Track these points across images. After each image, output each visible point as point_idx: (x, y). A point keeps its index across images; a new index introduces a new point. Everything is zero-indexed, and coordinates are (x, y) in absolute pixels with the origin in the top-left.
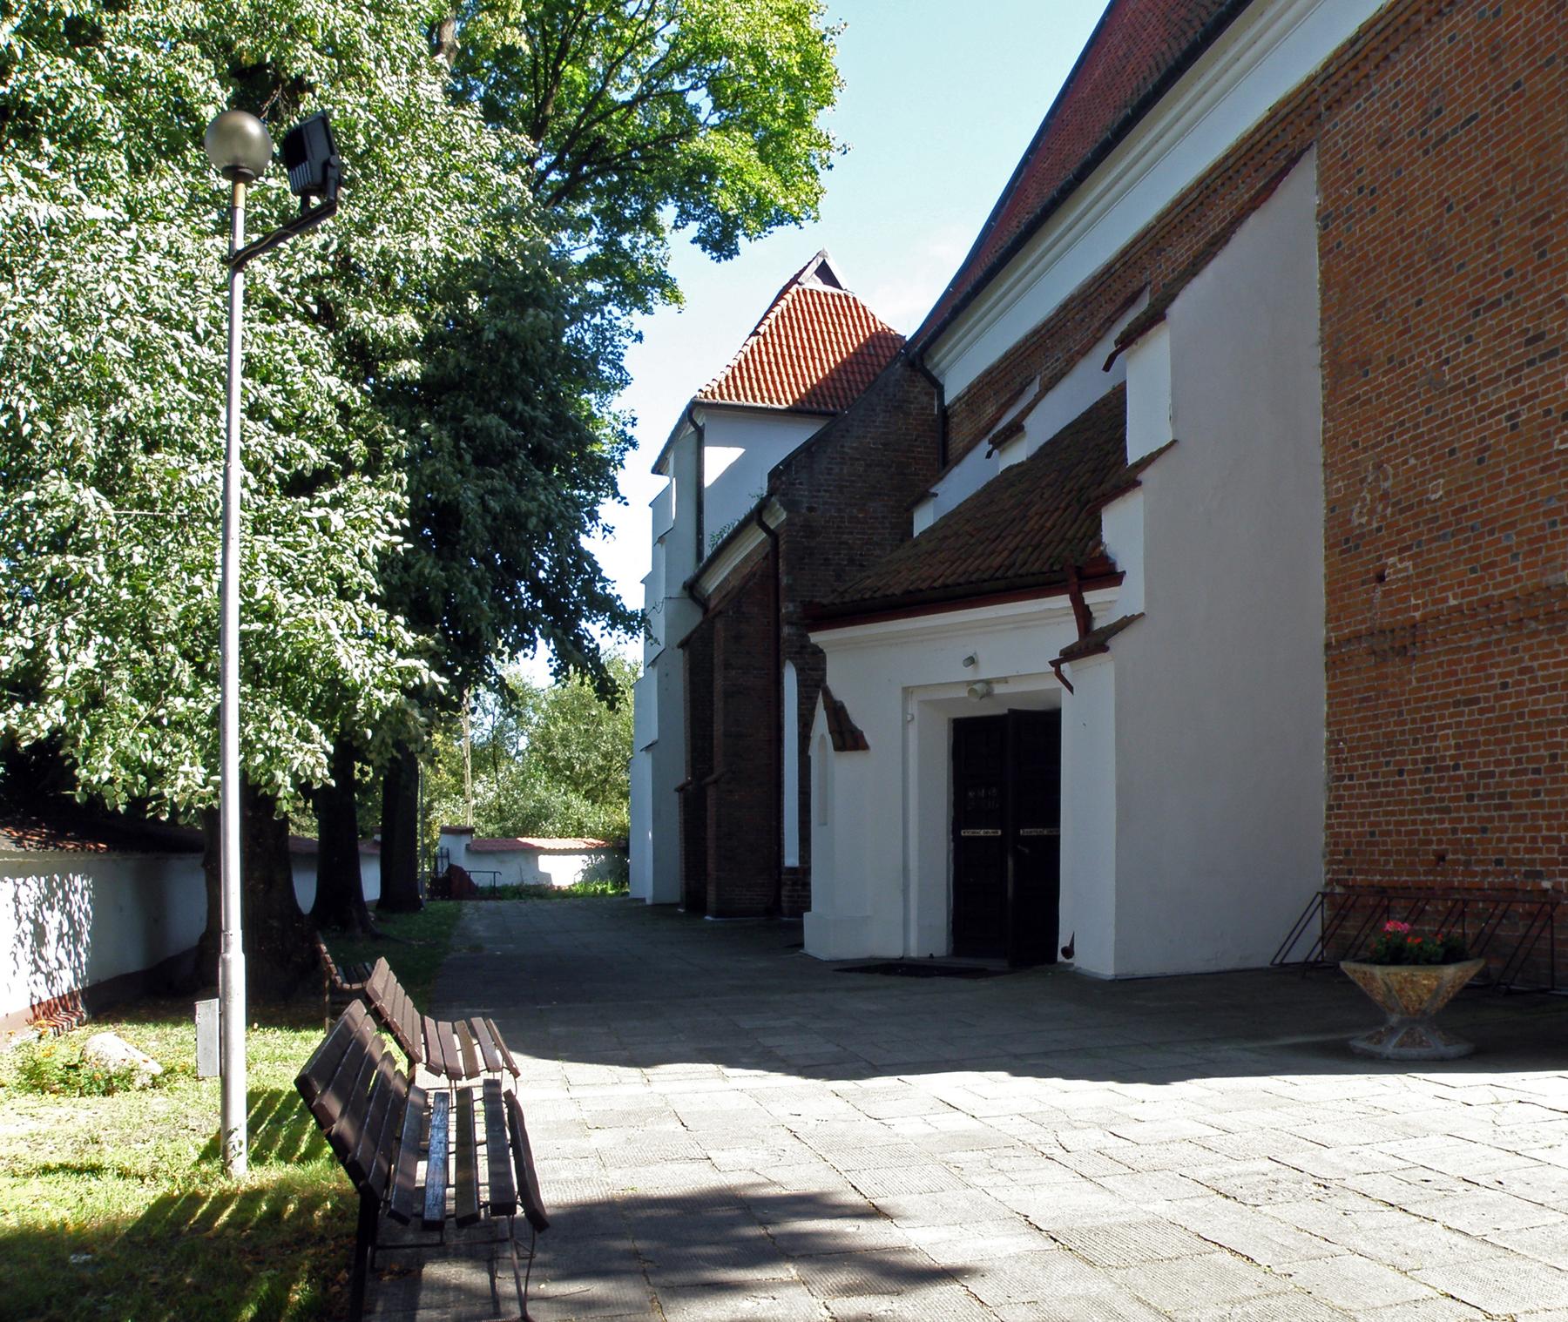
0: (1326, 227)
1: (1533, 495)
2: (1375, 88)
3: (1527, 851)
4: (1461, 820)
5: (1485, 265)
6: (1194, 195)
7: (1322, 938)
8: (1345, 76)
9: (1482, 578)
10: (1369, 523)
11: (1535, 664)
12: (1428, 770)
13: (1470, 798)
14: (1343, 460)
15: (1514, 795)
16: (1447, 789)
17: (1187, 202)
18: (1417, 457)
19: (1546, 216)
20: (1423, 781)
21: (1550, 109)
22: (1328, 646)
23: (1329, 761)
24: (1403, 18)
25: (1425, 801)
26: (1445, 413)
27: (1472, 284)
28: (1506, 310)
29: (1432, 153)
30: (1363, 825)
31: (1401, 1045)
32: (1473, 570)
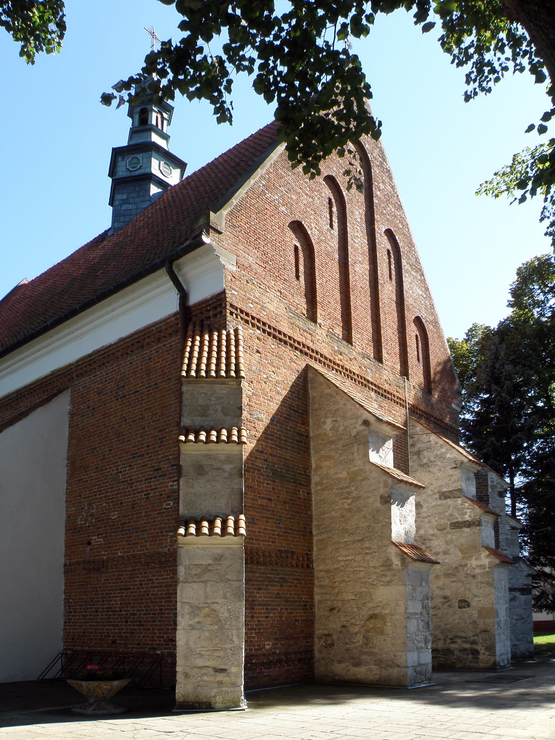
0: (72, 417)
1: (154, 522)
3: (150, 641)
4: (123, 629)
5: (139, 442)
6: (14, 396)
7: (61, 670)
8: (86, 367)
9: (132, 548)
10: (85, 524)
11: (154, 578)
12: (108, 611)
13: (127, 622)
14: (75, 500)
15: (145, 621)
16: (117, 618)
17: (11, 397)
18: (106, 503)
19: (165, 429)
20: (106, 615)
21: (169, 394)
22: (65, 565)
23: (65, 606)
25: (107, 622)
26: (119, 490)
27: (133, 447)
28: (146, 458)
30: (80, 629)
31: (95, 710)
32: (129, 544)
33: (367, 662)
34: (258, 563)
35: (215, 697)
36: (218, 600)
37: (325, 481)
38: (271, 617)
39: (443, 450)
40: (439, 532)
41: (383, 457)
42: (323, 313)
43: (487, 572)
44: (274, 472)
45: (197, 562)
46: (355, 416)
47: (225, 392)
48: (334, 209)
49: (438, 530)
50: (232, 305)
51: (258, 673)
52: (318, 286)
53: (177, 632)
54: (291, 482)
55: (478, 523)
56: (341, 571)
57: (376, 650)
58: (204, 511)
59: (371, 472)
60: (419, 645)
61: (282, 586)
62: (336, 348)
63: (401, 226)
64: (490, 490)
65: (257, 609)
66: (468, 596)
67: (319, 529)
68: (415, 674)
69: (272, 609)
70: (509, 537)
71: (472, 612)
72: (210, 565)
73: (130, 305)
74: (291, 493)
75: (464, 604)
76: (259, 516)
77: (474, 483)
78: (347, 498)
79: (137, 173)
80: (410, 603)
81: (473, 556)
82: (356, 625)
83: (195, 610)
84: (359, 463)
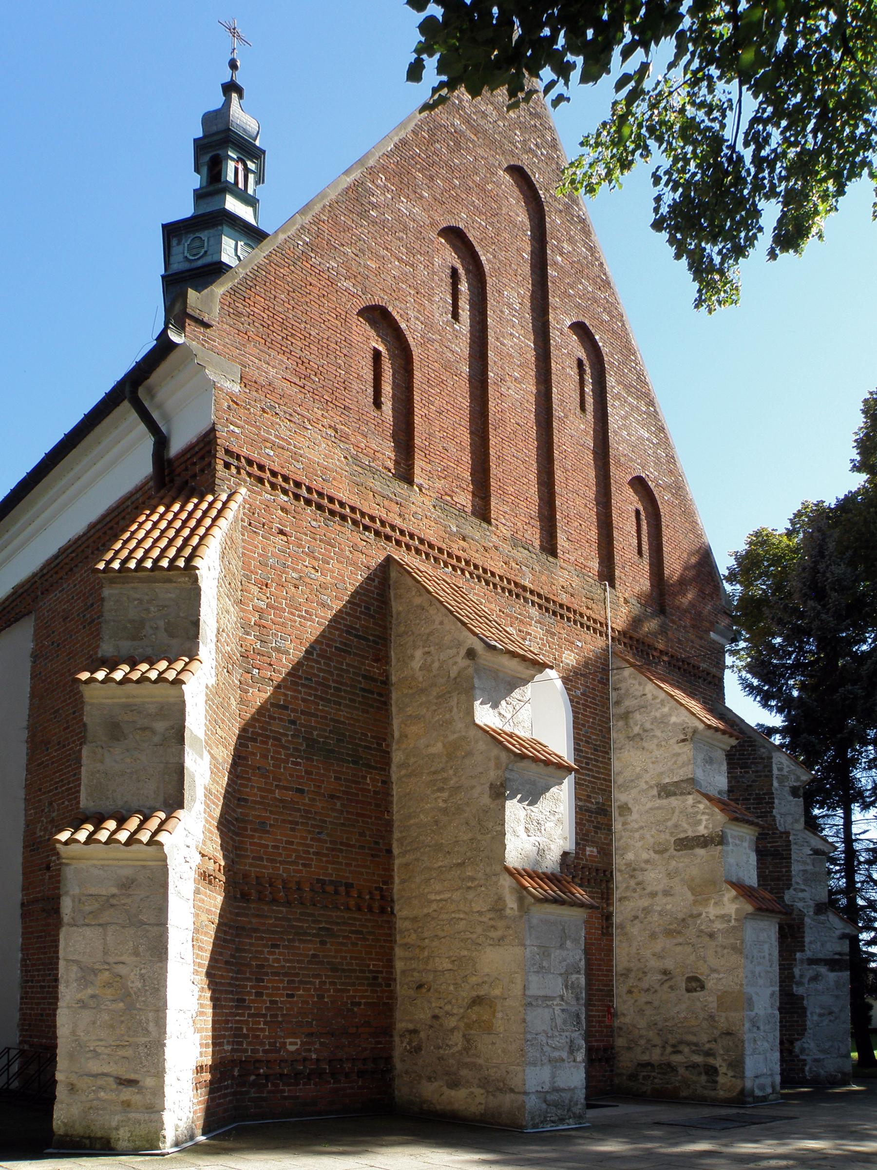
0: (34, 662)
2: (65, 586)
8: (52, 576)
22: (23, 904)
23: (22, 971)
24: (81, 549)
29: (87, 628)
33: (467, 1082)
34: (275, 901)
35: (117, 1129)
36: (124, 958)
37: (412, 760)
38: (301, 996)
39: (666, 710)
40: (656, 857)
41: (509, 716)
42: (428, 467)
43: (734, 927)
44: (311, 743)
45: (93, 890)
46: (456, 642)
47: (173, 596)
48: (464, 287)
49: (656, 852)
50: (228, 452)
51: (269, 1092)
52: (417, 420)
53: (59, 1011)
54: (348, 762)
55: (721, 840)
56: (433, 918)
57: (480, 1061)
58: (120, 803)
59: (477, 742)
60: (556, 1054)
61: (323, 943)
62: (455, 529)
63: (606, 317)
64: (775, 784)
65: (269, 981)
66: (702, 971)
67: (402, 844)
68: (544, 1106)
69: (301, 982)
70: (809, 868)
71: (707, 999)
72: (113, 896)
73: (99, 465)
74: (346, 780)
75: (695, 984)
76: (276, 820)
77: (724, 767)
78: (442, 790)
79: (200, 263)
80: (533, 978)
81: (708, 899)
82: (453, 1015)
83: (88, 974)
84: (460, 725)
